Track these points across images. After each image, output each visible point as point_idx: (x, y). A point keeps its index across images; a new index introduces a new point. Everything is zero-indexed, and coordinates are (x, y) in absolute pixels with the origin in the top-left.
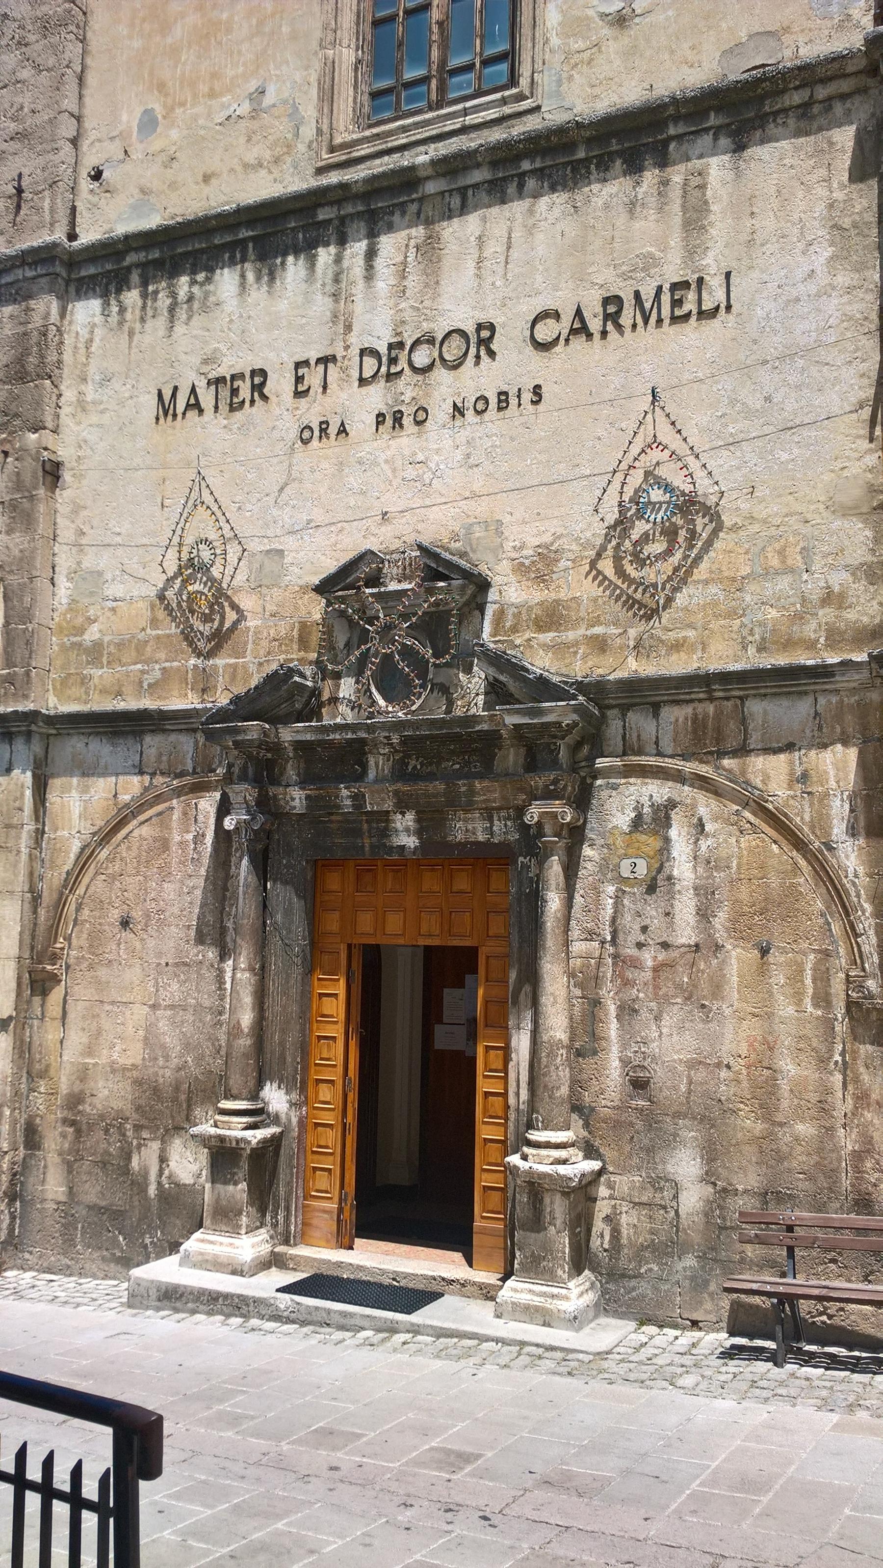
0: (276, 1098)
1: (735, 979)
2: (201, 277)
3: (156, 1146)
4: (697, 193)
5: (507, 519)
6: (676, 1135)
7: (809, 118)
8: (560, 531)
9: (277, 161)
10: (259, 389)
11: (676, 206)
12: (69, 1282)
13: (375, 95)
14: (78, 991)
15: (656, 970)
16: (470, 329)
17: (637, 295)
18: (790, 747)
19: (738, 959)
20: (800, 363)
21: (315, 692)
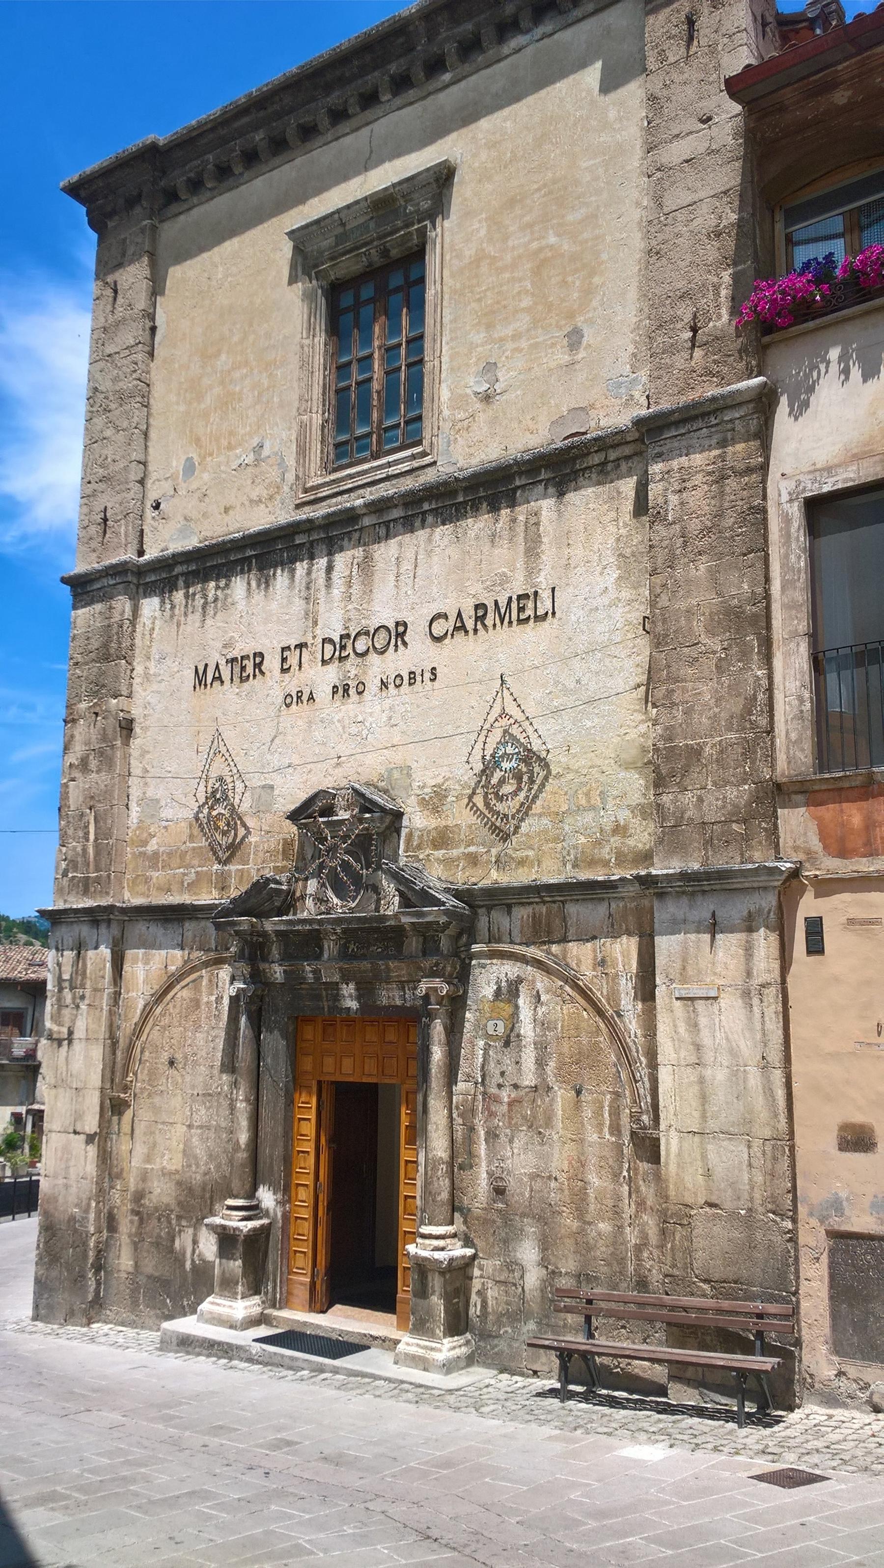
0: (267, 1197)
1: (560, 1112)
2: (222, 583)
3: (191, 1231)
4: (533, 528)
5: (414, 765)
6: (522, 1230)
7: (605, 472)
8: (448, 775)
9: (271, 498)
10: (258, 666)
11: (520, 538)
12: (130, 1332)
13: (337, 446)
14: (141, 1113)
15: (510, 1104)
16: (391, 625)
17: (496, 602)
18: (594, 938)
19: (562, 1098)
20: (599, 655)
21: (290, 893)
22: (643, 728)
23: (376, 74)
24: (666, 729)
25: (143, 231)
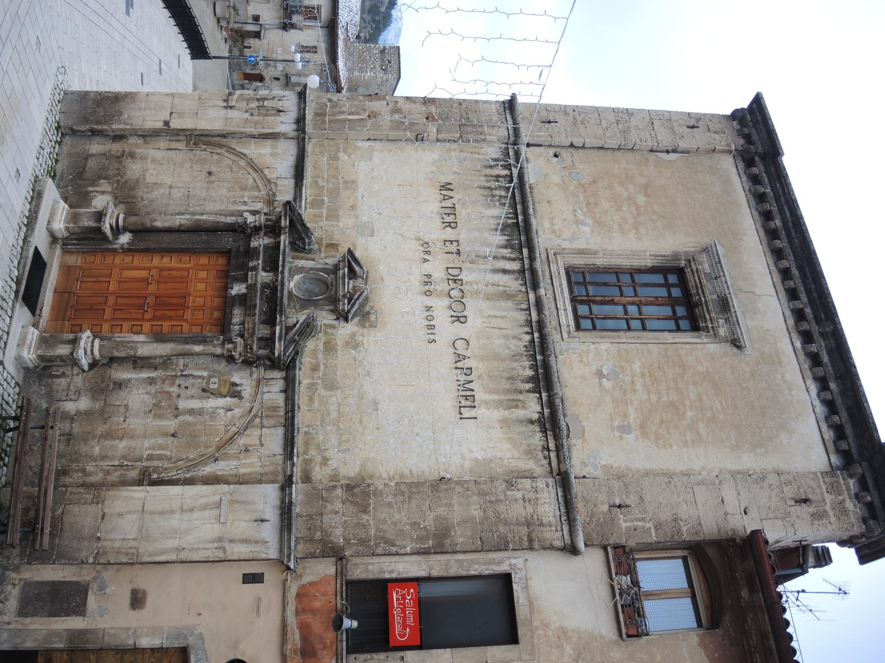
0: (125, 239)
3: (110, 189)
6: (97, 400)
14: (182, 154)
17: (471, 382)
20: (432, 447)
22: (385, 475)
23: (806, 299)
24: (381, 492)
25: (728, 145)
